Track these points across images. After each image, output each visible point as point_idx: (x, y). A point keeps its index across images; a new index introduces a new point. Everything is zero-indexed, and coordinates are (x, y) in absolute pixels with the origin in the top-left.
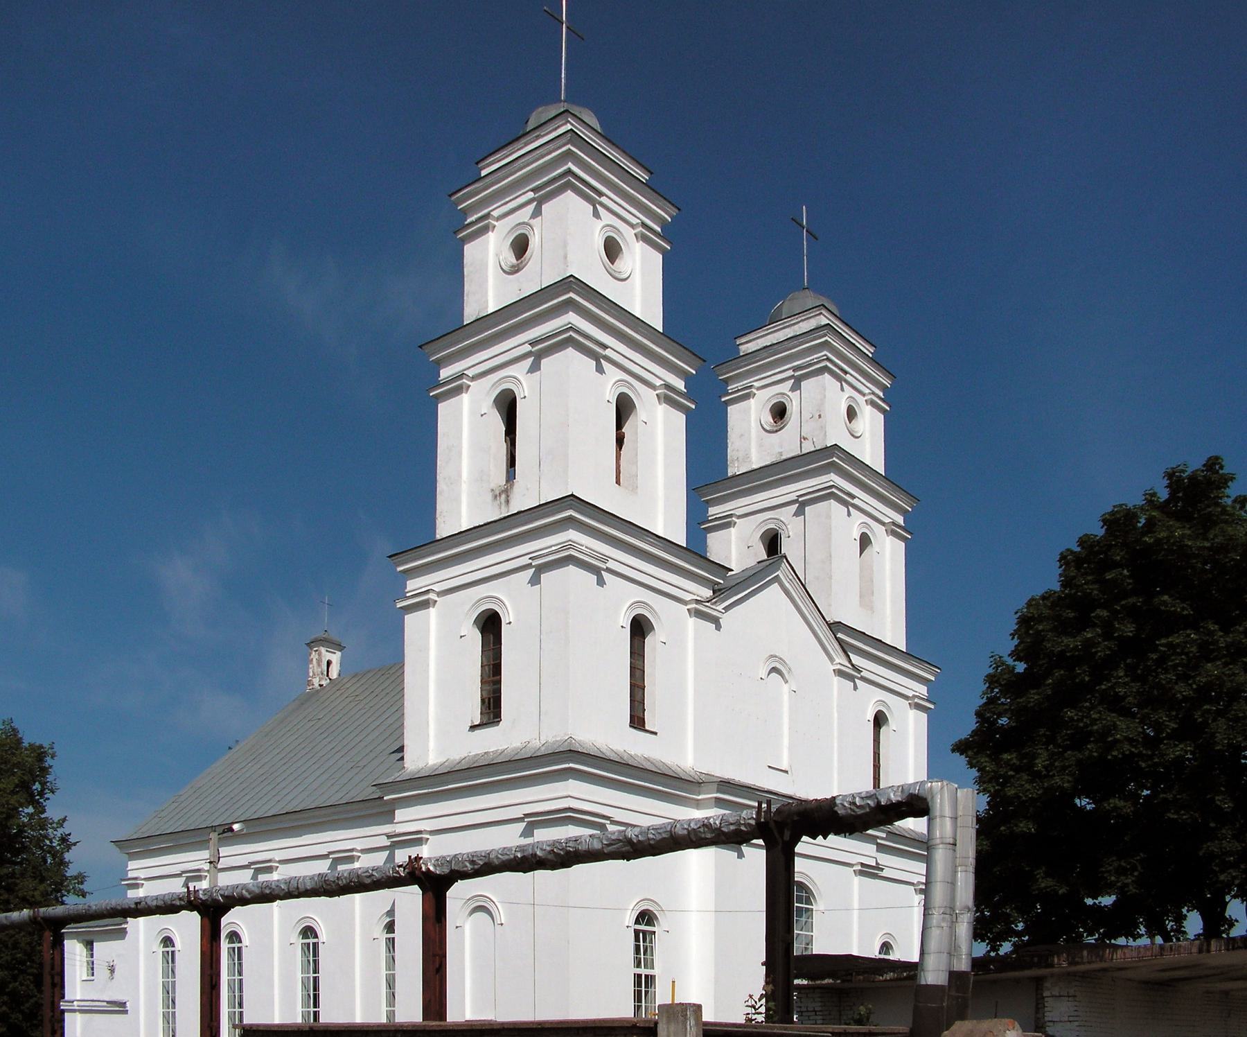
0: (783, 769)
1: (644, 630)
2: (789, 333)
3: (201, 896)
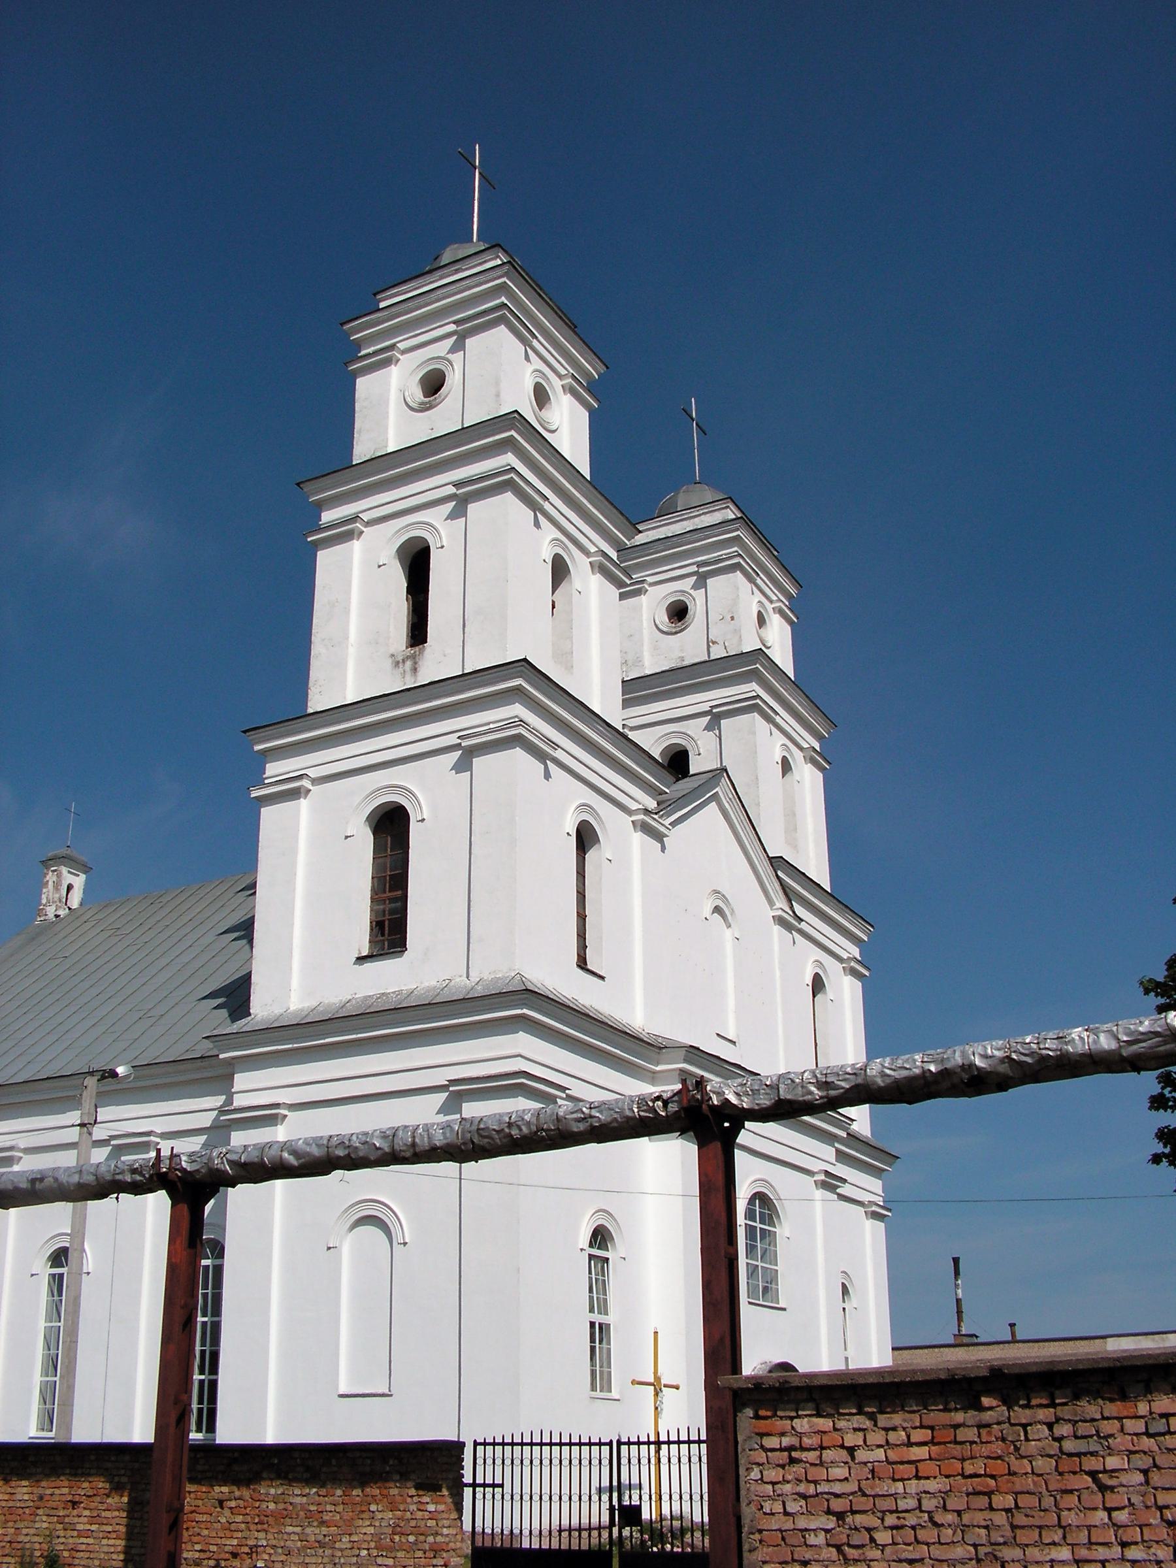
0: (730, 1038)
1: (586, 844)
2: (688, 526)
3: (184, 1164)
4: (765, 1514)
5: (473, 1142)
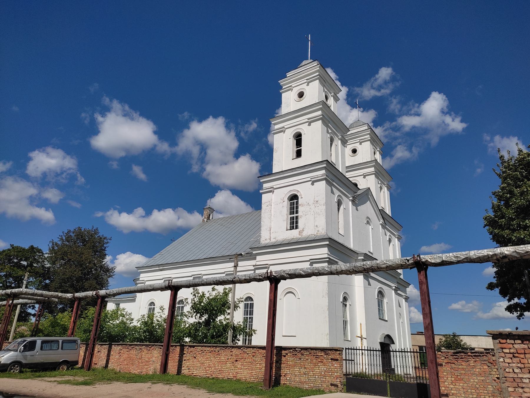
3: (274, 274)
4: (506, 372)
5: (353, 269)
